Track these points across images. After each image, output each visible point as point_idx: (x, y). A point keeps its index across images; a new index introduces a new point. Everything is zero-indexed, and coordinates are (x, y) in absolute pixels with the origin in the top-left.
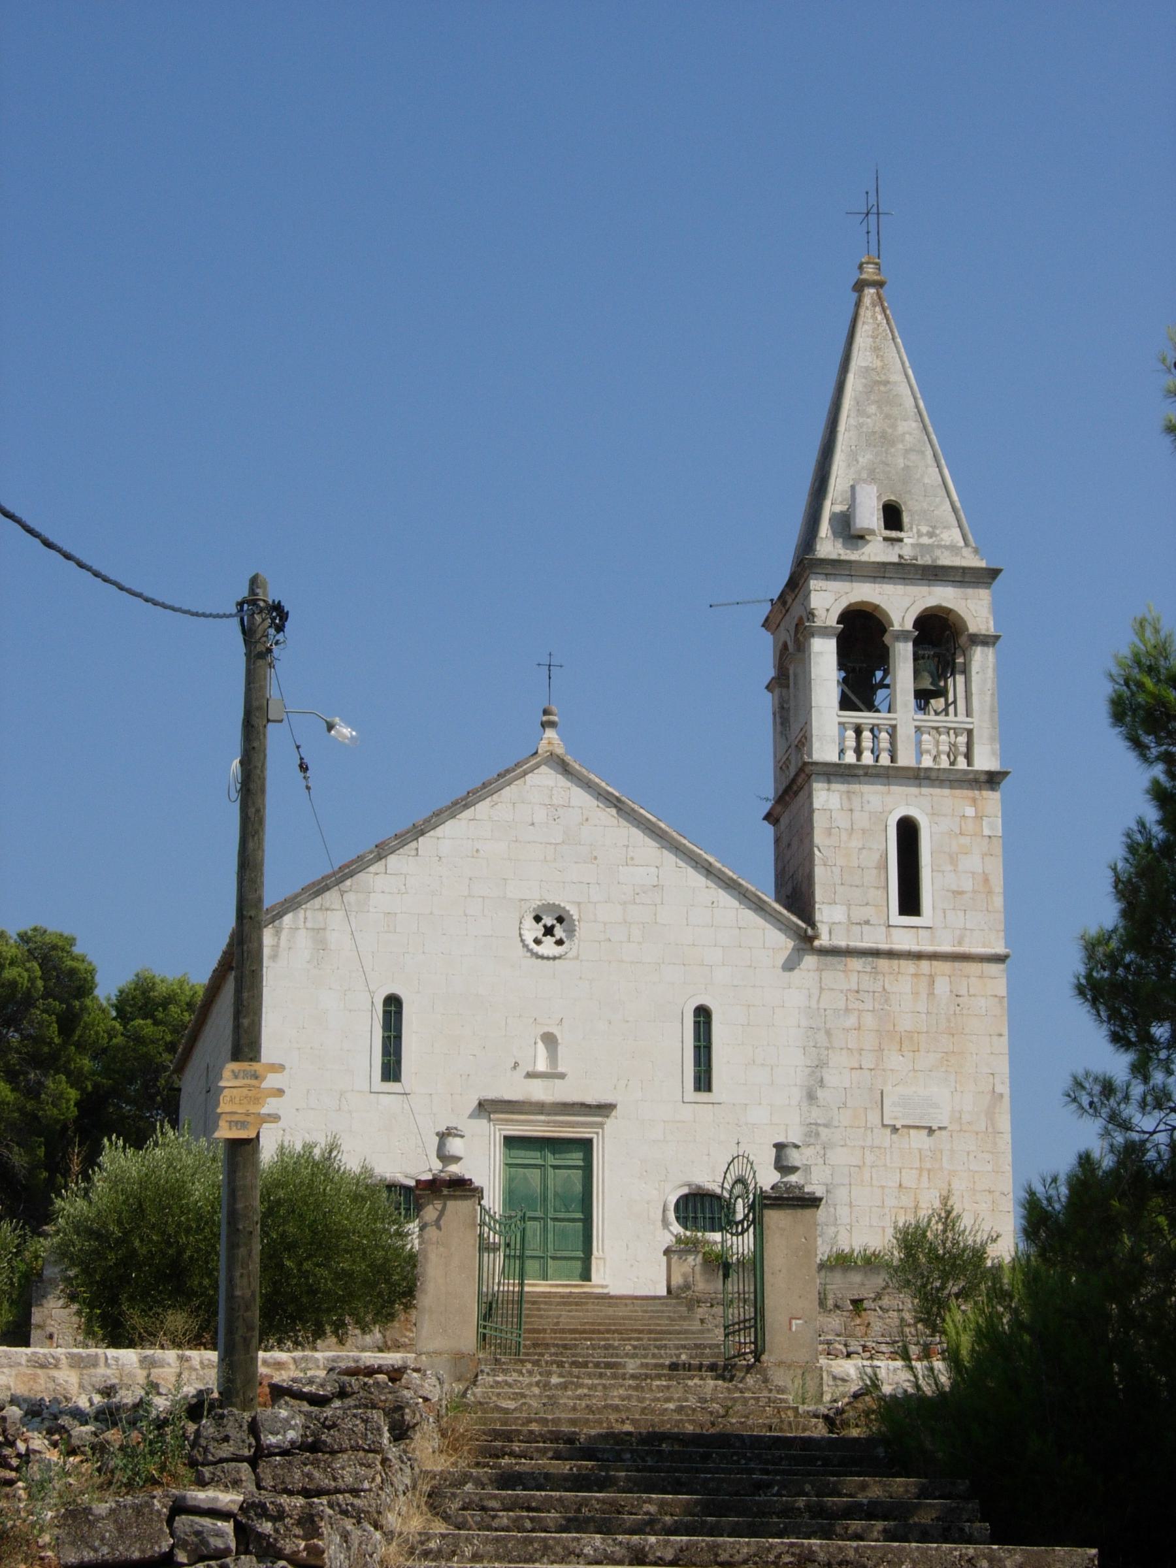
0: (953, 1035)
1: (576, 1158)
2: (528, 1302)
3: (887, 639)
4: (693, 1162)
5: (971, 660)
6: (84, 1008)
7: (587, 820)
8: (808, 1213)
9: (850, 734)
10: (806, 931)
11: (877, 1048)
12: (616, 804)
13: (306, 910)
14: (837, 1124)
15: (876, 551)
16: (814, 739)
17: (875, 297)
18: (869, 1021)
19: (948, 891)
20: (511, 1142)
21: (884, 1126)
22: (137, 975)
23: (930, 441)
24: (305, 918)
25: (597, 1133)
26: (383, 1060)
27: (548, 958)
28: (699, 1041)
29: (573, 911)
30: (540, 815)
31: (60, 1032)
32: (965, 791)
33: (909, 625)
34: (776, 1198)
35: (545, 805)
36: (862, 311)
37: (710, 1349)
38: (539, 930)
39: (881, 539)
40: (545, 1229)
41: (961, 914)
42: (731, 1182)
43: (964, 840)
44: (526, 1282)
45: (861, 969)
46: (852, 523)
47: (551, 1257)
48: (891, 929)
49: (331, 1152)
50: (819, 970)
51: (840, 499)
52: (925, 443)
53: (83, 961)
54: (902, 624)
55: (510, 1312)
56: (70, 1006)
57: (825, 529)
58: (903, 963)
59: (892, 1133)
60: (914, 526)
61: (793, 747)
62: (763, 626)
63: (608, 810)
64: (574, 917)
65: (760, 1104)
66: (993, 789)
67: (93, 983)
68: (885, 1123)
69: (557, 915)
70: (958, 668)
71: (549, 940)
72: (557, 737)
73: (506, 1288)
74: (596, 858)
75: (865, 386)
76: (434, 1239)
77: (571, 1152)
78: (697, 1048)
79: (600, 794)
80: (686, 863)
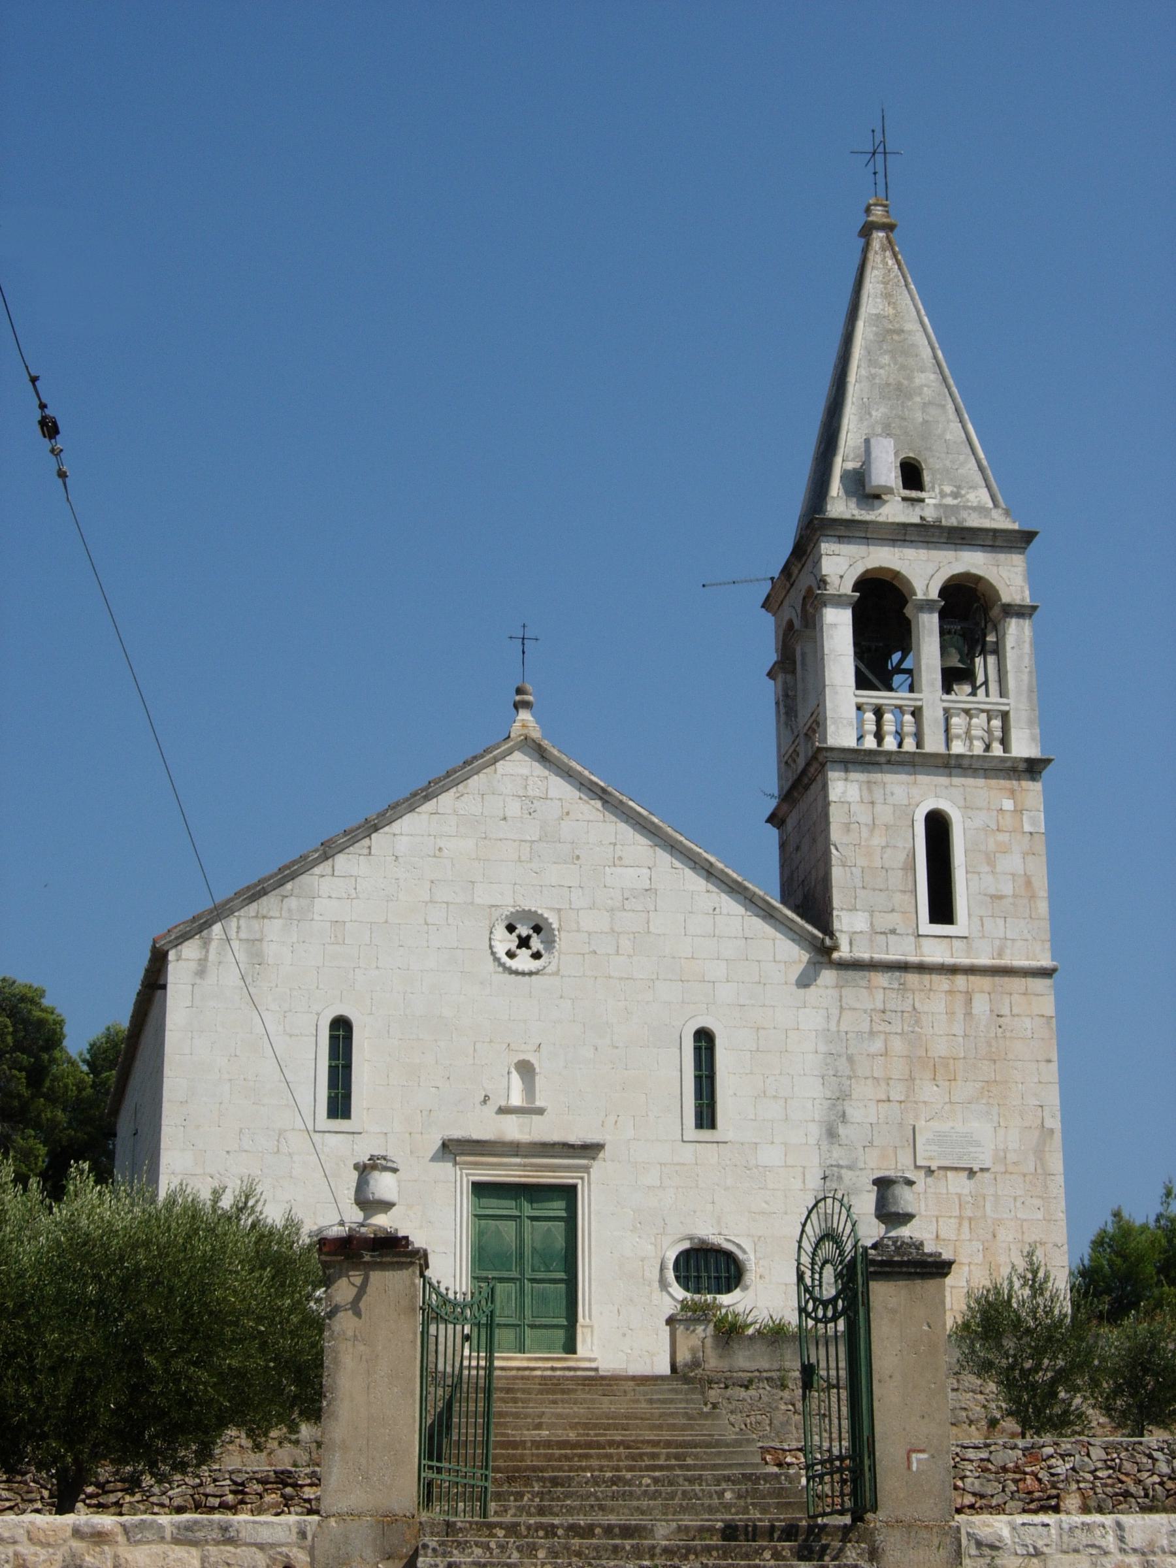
0: (995, 1061)
1: (557, 1207)
2: (501, 1390)
3: (909, 611)
4: (695, 1212)
5: (1005, 634)
6: (53, 1060)
7: (568, 813)
8: (931, 1284)
9: (870, 716)
10: (823, 940)
11: (906, 1077)
12: (601, 795)
13: (238, 918)
14: (862, 1166)
15: (894, 511)
16: (829, 722)
17: (885, 242)
18: (897, 1045)
19: (985, 895)
20: (480, 1189)
21: (917, 1167)
22: (108, 1029)
23: (951, 394)
24: (238, 928)
25: (582, 1178)
26: (330, 1093)
27: (523, 974)
28: (701, 1070)
29: (553, 919)
30: (514, 808)
31: (28, 1085)
32: (1002, 782)
33: (934, 594)
34: (882, 1263)
35: (519, 797)
36: (871, 256)
37: (766, 1481)
38: (512, 942)
39: (900, 499)
40: (522, 1290)
41: (1001, 922)
42: (813, 1240)
43: (1003, 837)
44: (496, 1355)
45: (886, 985)
46: (867, 480)
47: (529, 1326)
48: (921, 938)
49: (247, 1197)
50: (838, 986)
51: (852, 456)
52: (945, 396)
53: (52, 1013)
54: (926, 593)
55: (471, 1438)
56: (37, 1058)
57: (836, 487)
58: (935, 978)
59: (926, 1176)
60: (936, 486)
61: (802, 735)
62: (763, 606)
63: (592, 802)
64: (554, 926)
65: (772, 1143)
66: (1033, 779)
67: (62, 1034)
68: (918, 1164)
69: (533, 924)
70: (989, 647)
71: (524, 953)
72: (531, 719)
73: (474, 1363)
74: (578, 857)
75: (876, 334)
76: (350, 1333)
77: (552, 1200)
78: (698, 1079)
79: (582, 784)
80: (682, 863)
